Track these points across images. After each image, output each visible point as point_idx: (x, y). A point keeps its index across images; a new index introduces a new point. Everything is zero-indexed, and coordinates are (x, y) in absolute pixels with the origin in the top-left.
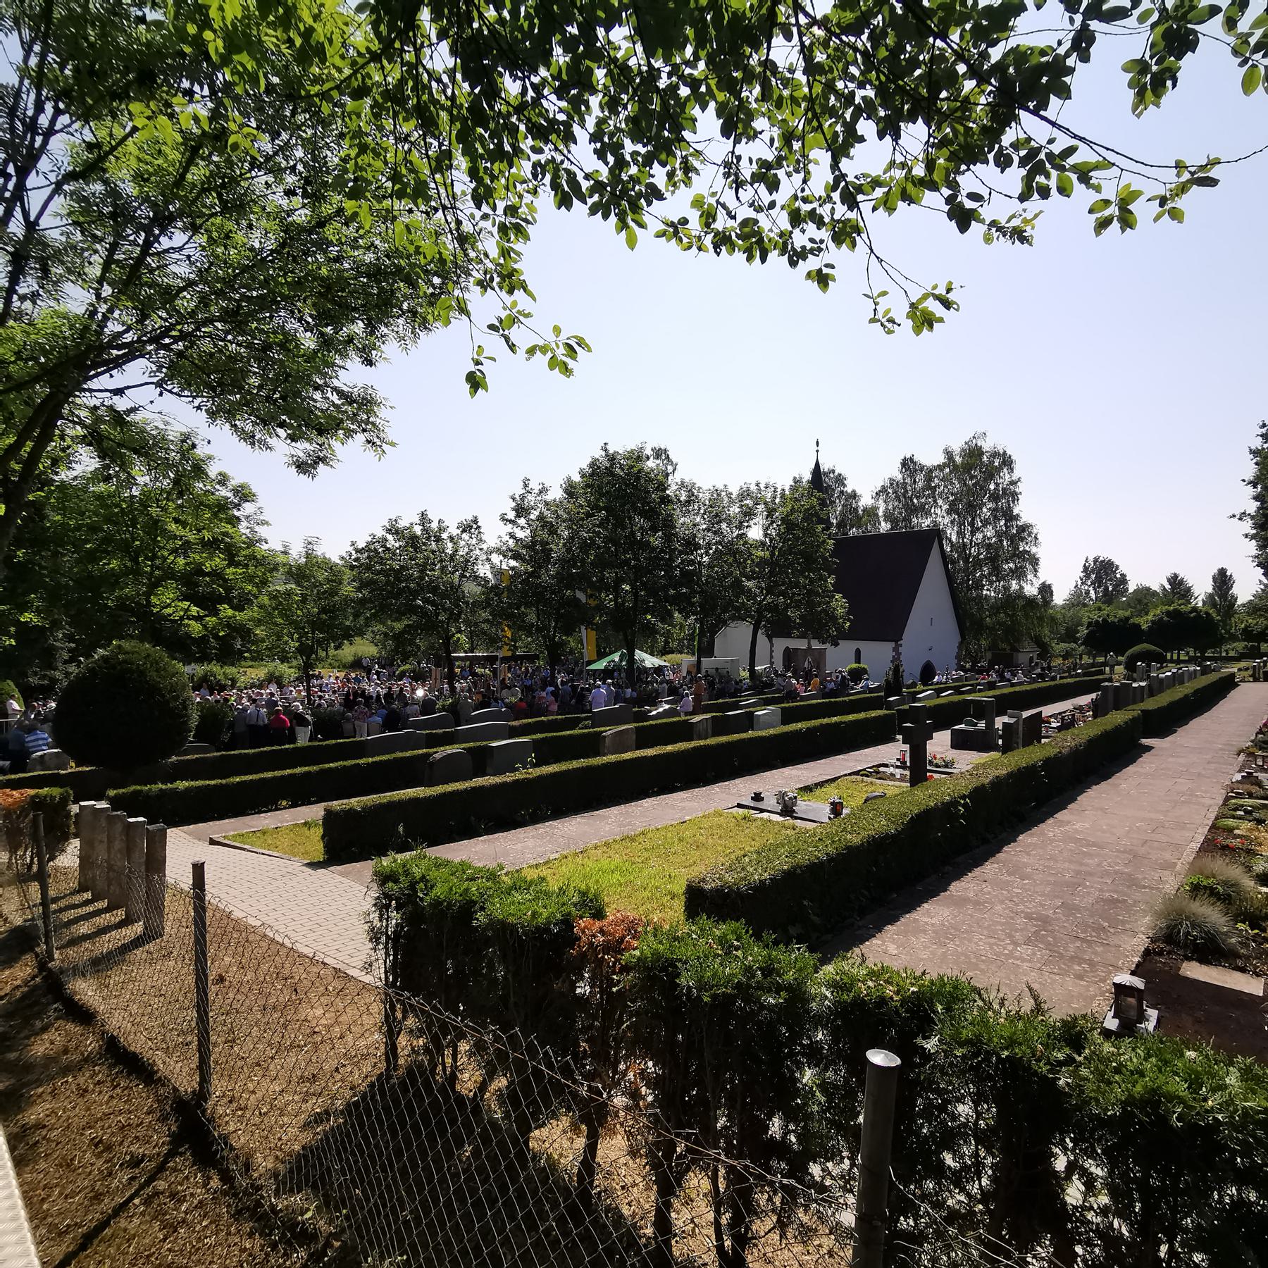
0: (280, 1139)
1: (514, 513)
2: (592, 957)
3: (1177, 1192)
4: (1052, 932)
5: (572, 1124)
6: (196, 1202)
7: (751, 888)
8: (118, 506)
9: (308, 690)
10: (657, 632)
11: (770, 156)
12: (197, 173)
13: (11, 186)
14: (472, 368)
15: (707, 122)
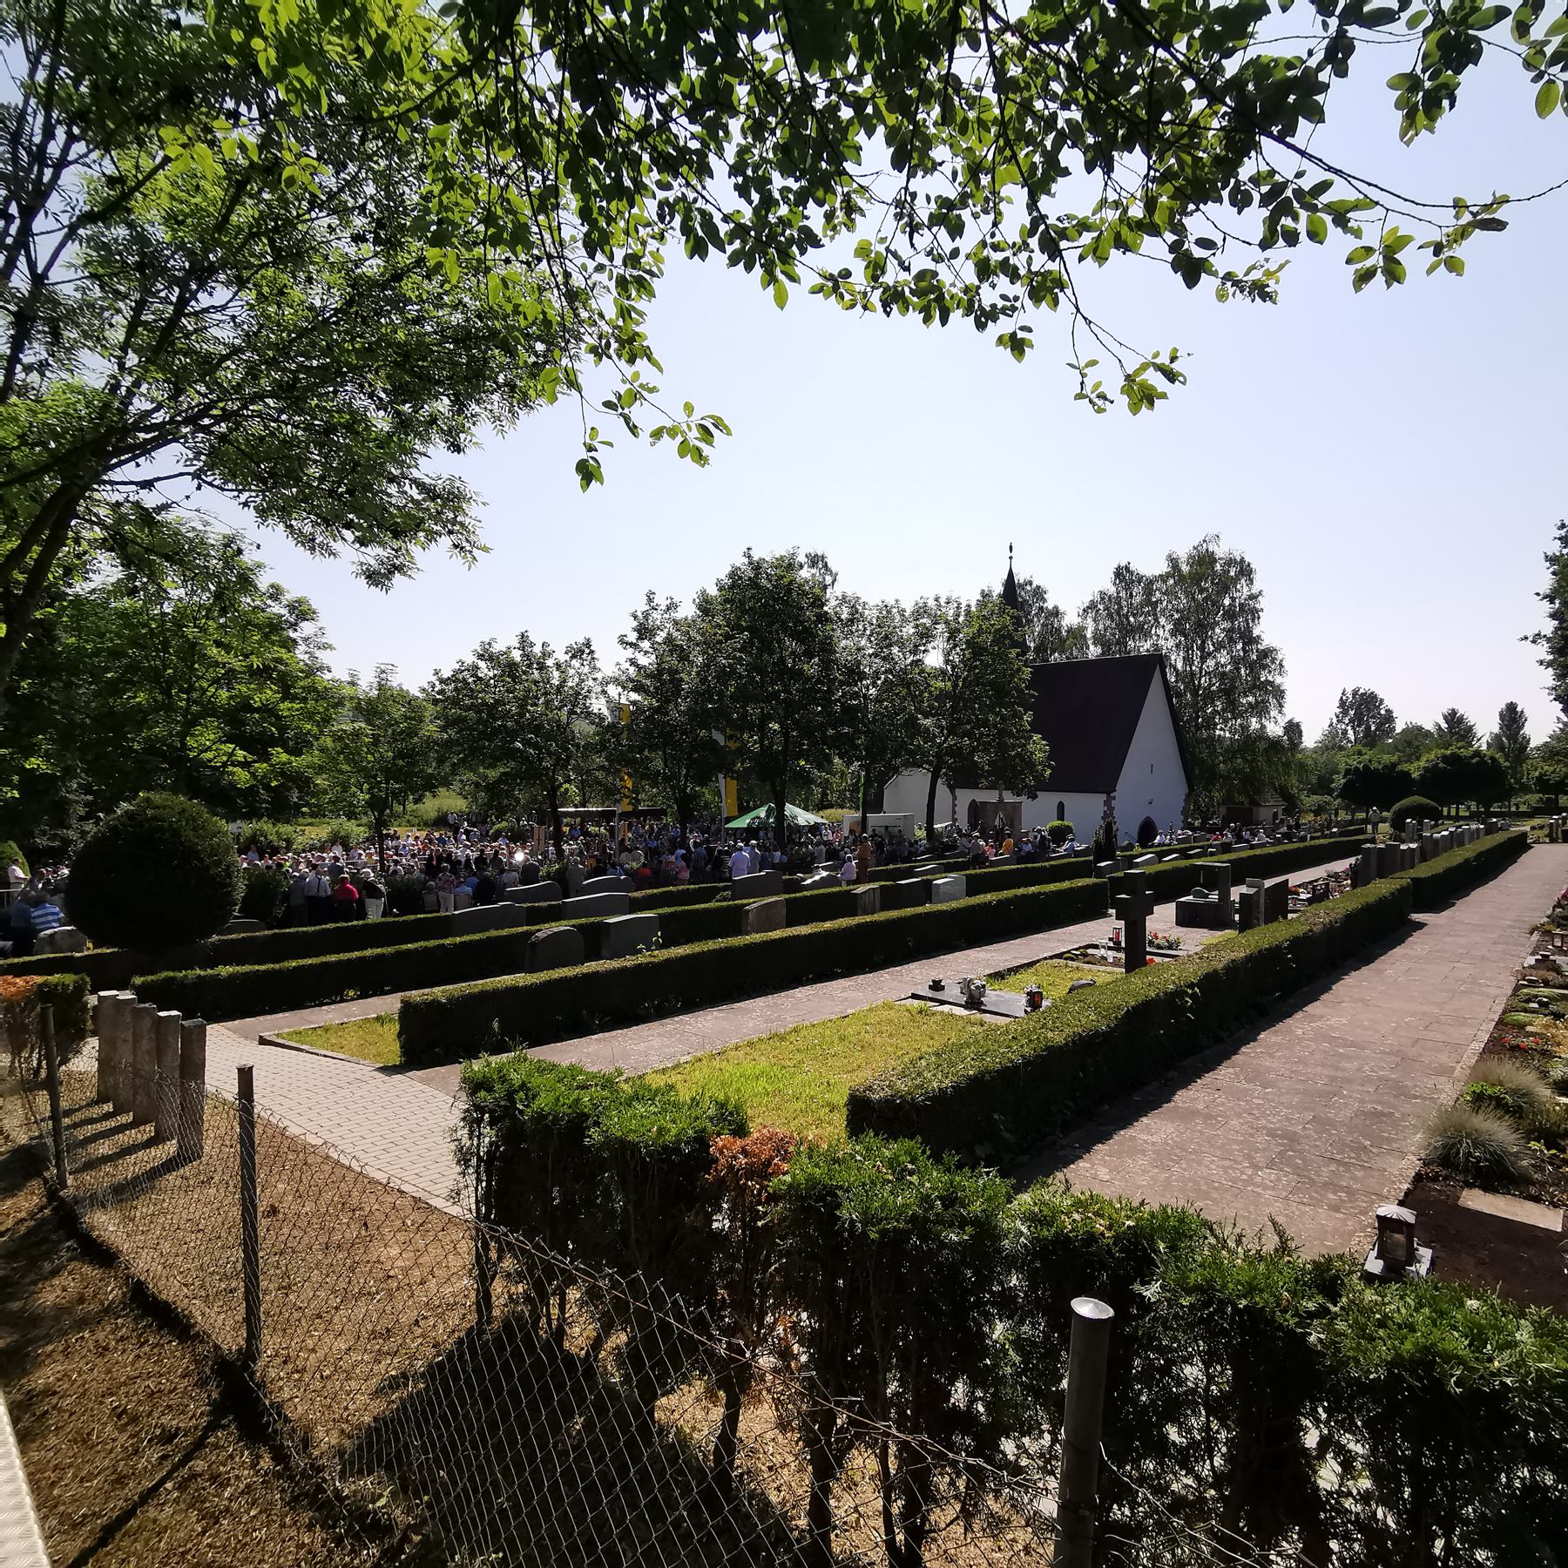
0: (346, 1408)
1: (635, 635)
2: (732, 1184)
3: (1455, 1474)
4: (1301, 1152)
5: (707, 1390)
6: (242, 1486)
7: (928, 1099)
8: (145, 625)
9: (381, 854)
10: (812, 781)
11: (952, 193)
12: (244, 214)
13: (13, 230)
14: (584, 455)
15: (874, 151)
